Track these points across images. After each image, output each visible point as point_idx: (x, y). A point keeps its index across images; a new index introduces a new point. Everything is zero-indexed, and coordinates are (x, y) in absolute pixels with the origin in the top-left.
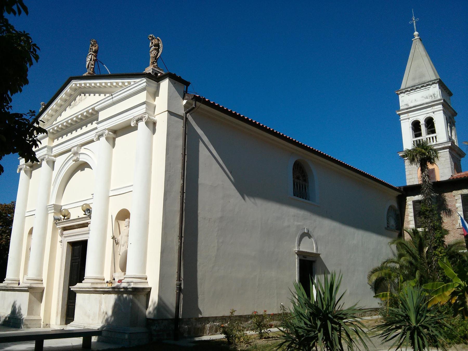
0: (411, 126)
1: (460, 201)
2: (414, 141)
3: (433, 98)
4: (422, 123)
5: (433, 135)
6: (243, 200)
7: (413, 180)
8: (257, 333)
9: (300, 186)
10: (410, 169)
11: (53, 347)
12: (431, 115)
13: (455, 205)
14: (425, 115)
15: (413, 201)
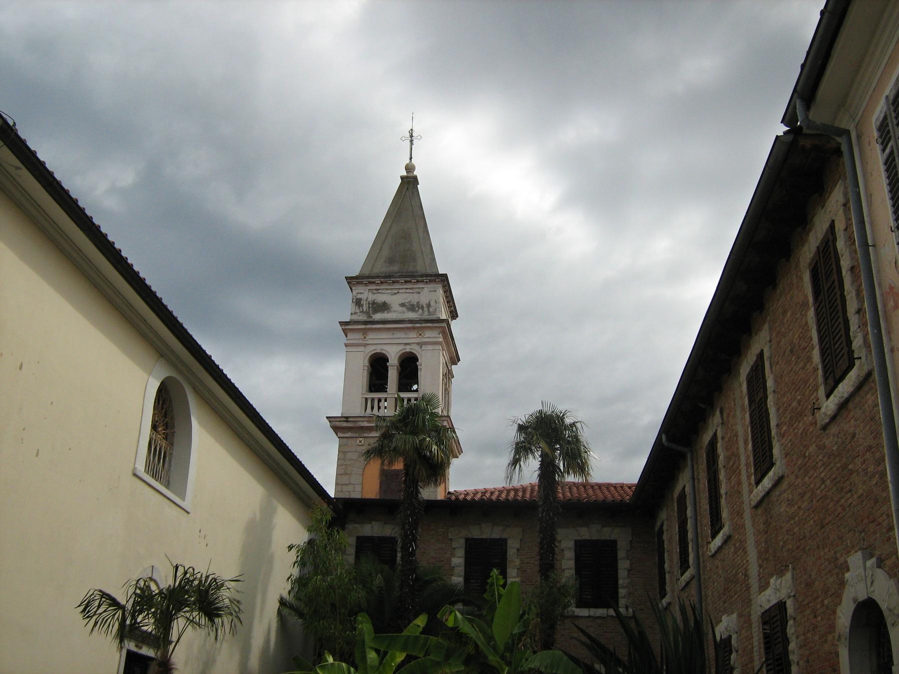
0: (367, 363)
1: (461, 552)
2: (366, 399)
3: (426, 313)
4: (393, 362)
5: (381, 395)
6: (508, 457)
7: (350, 488)
8: (735, 616)
9: (155, 449)
10: (348, 463)
11: (277, 627)
12: (415, 350)
13: (449, 561)
14: (402, 347)
15: (358, 538)
